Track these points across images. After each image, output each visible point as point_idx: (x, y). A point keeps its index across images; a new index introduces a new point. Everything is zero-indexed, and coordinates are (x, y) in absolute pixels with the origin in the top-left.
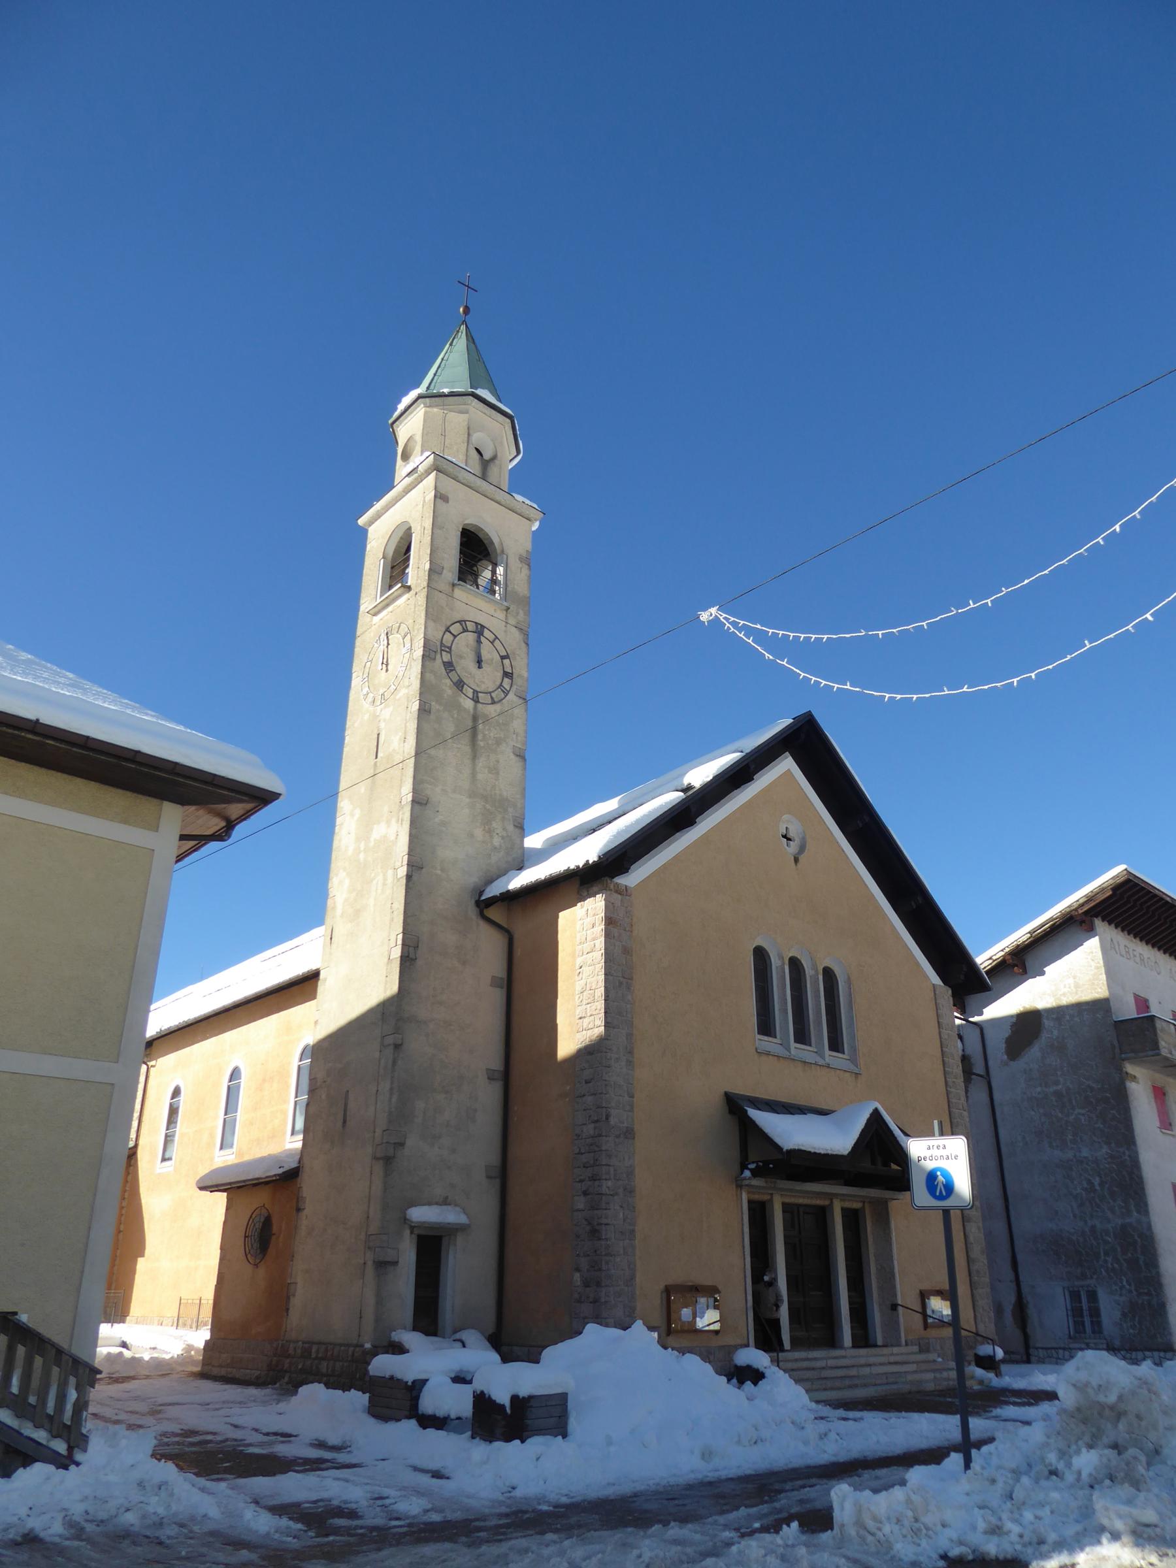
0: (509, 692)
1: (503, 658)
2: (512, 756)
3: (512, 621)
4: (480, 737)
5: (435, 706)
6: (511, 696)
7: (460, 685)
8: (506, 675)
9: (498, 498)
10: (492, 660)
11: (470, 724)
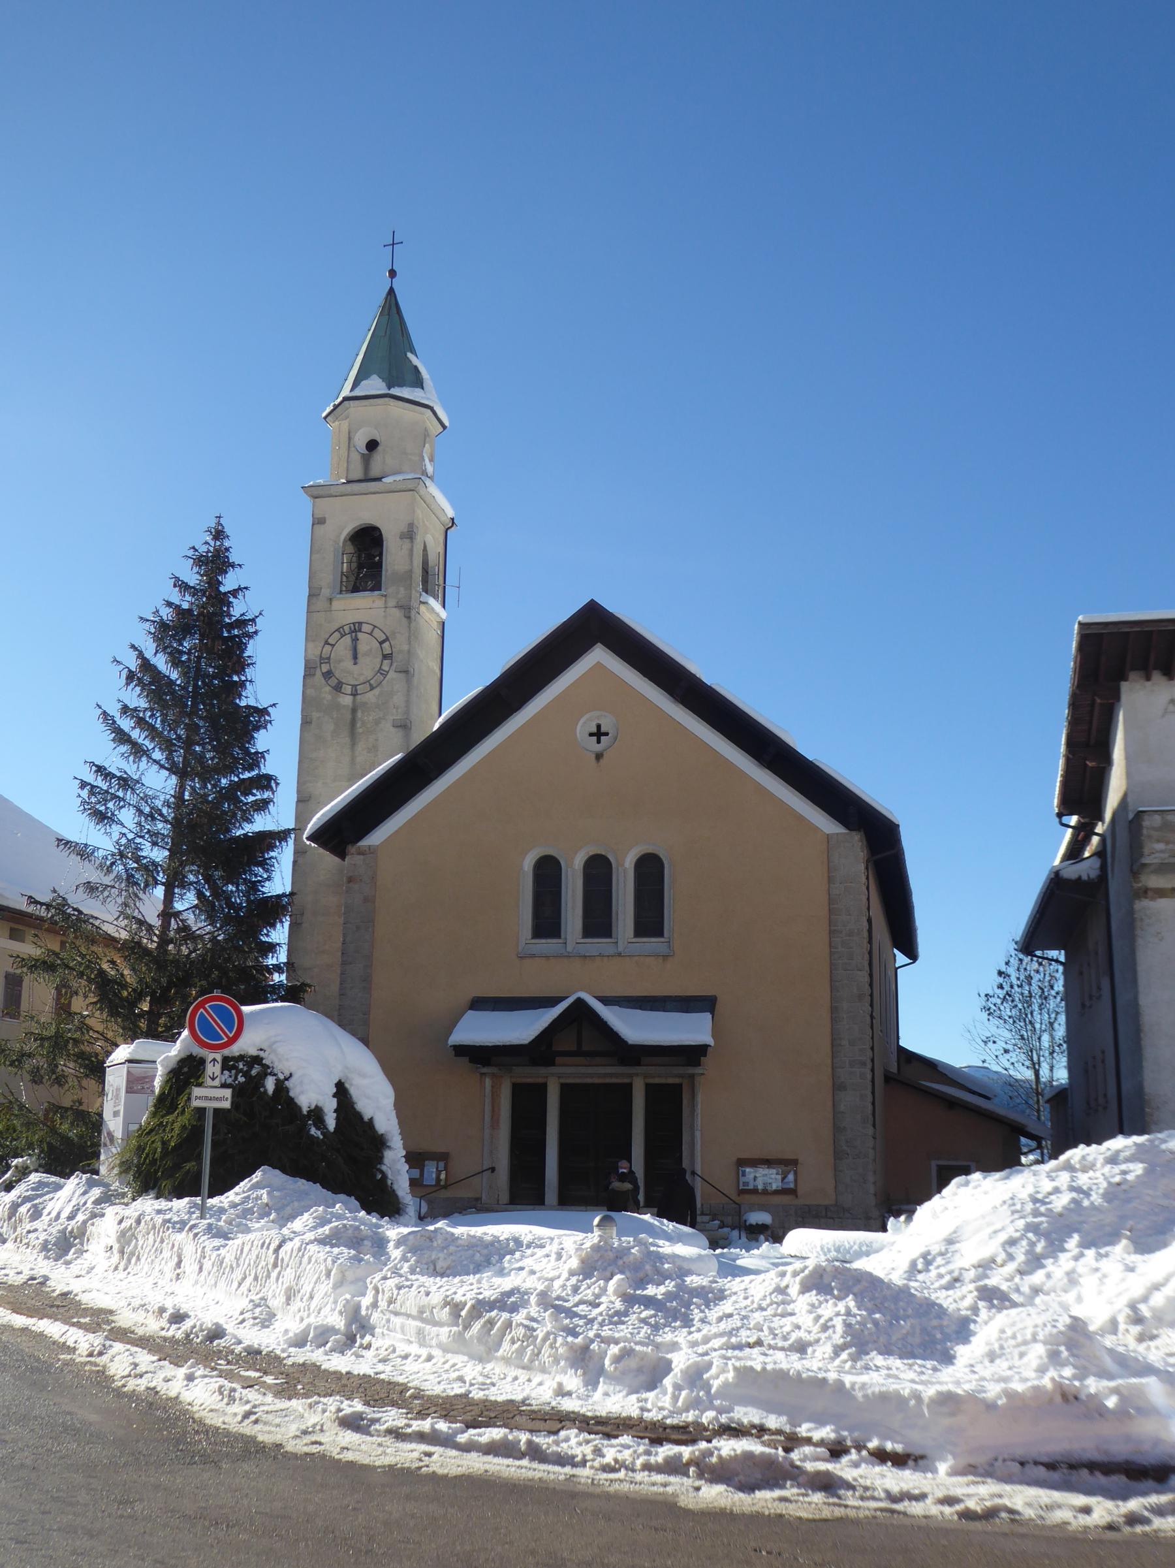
0: (388, 672)
1: (381, 643)
2: (393, 730)
4: (359, 725)
5: (315, 715)
6: (392, 675)
7: (338, 688)
8: (385, 657)
9: (372, 490)
10: (371, 650)
11: (349, 716)
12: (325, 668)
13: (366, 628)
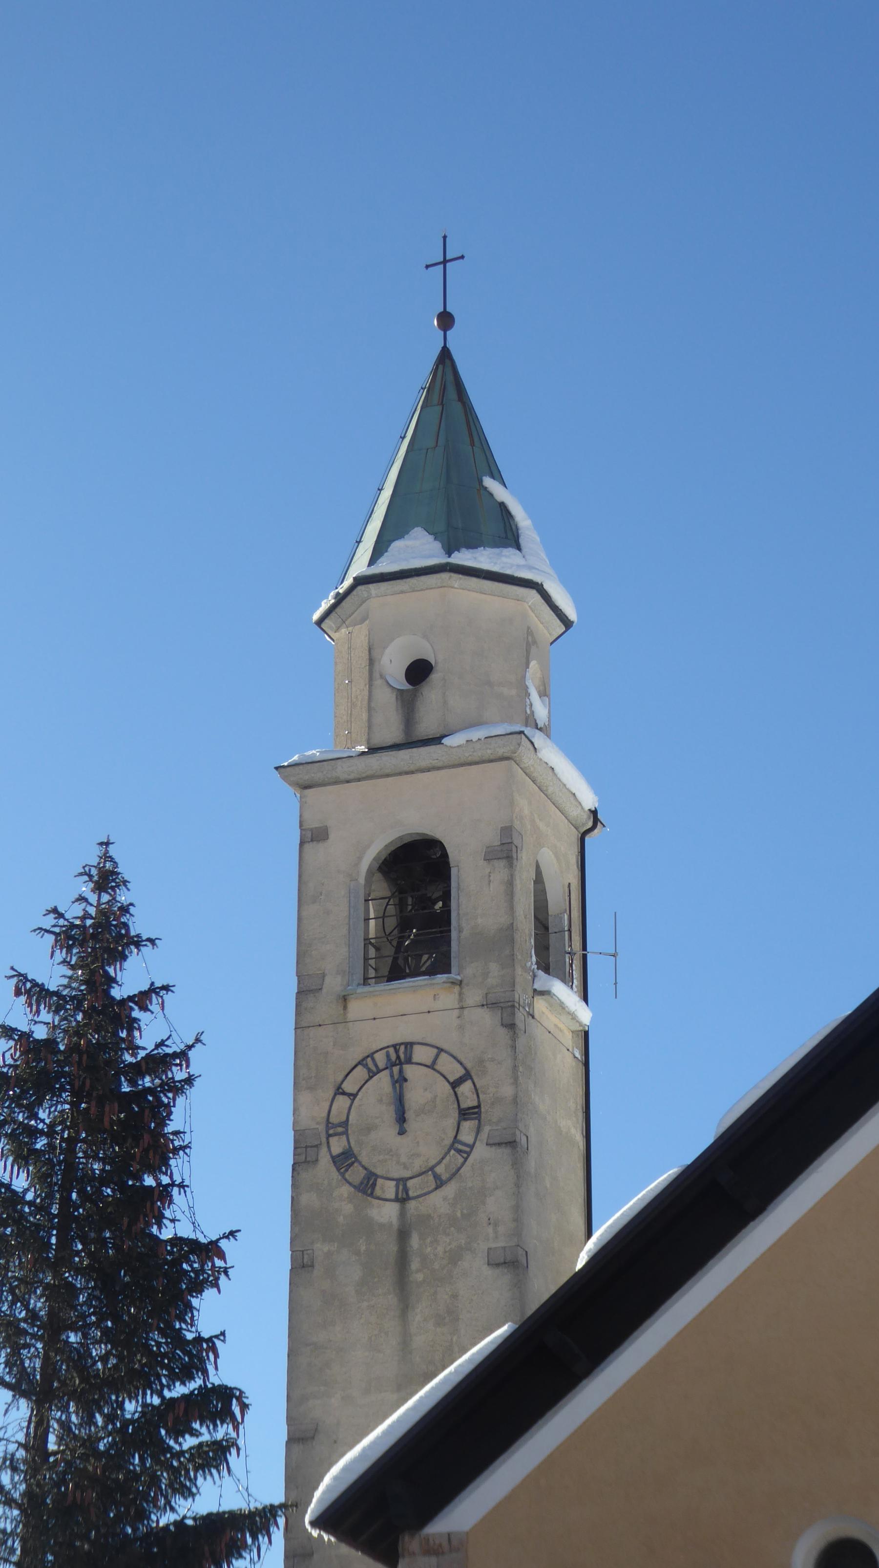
3: (473, 996)
4: (415, 1264)
5: (321, 1248)
6: (481, 1151)
8: (465, 1114)
12: (338, 1146)
13: (421, 1054)
